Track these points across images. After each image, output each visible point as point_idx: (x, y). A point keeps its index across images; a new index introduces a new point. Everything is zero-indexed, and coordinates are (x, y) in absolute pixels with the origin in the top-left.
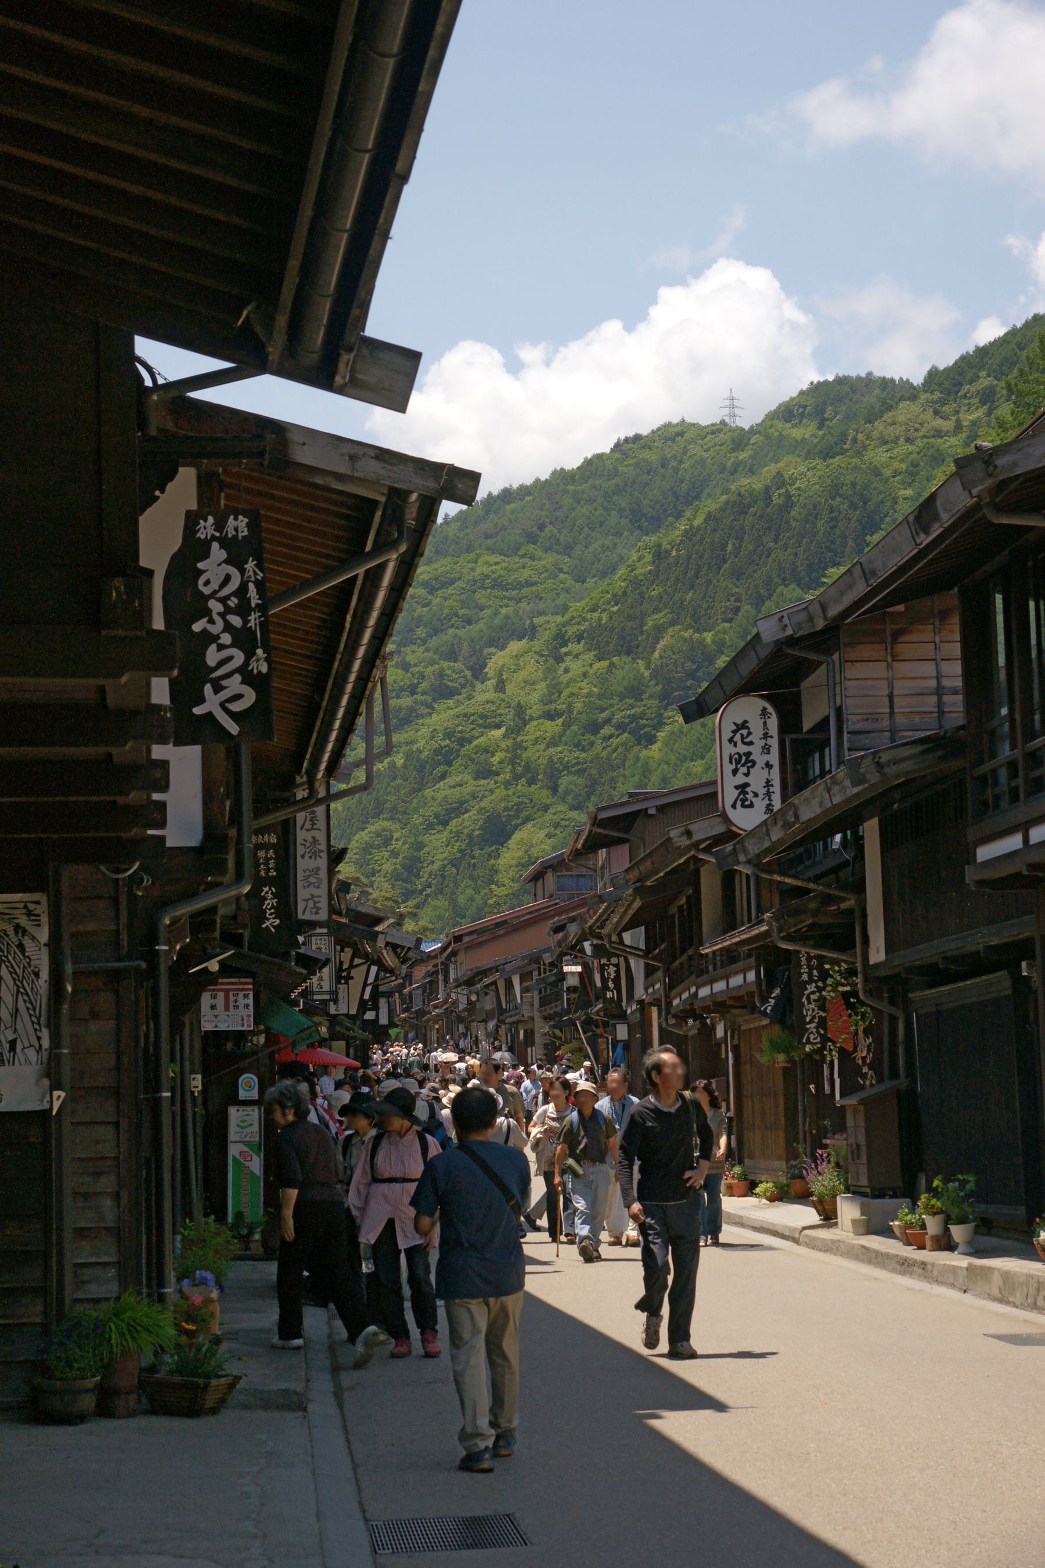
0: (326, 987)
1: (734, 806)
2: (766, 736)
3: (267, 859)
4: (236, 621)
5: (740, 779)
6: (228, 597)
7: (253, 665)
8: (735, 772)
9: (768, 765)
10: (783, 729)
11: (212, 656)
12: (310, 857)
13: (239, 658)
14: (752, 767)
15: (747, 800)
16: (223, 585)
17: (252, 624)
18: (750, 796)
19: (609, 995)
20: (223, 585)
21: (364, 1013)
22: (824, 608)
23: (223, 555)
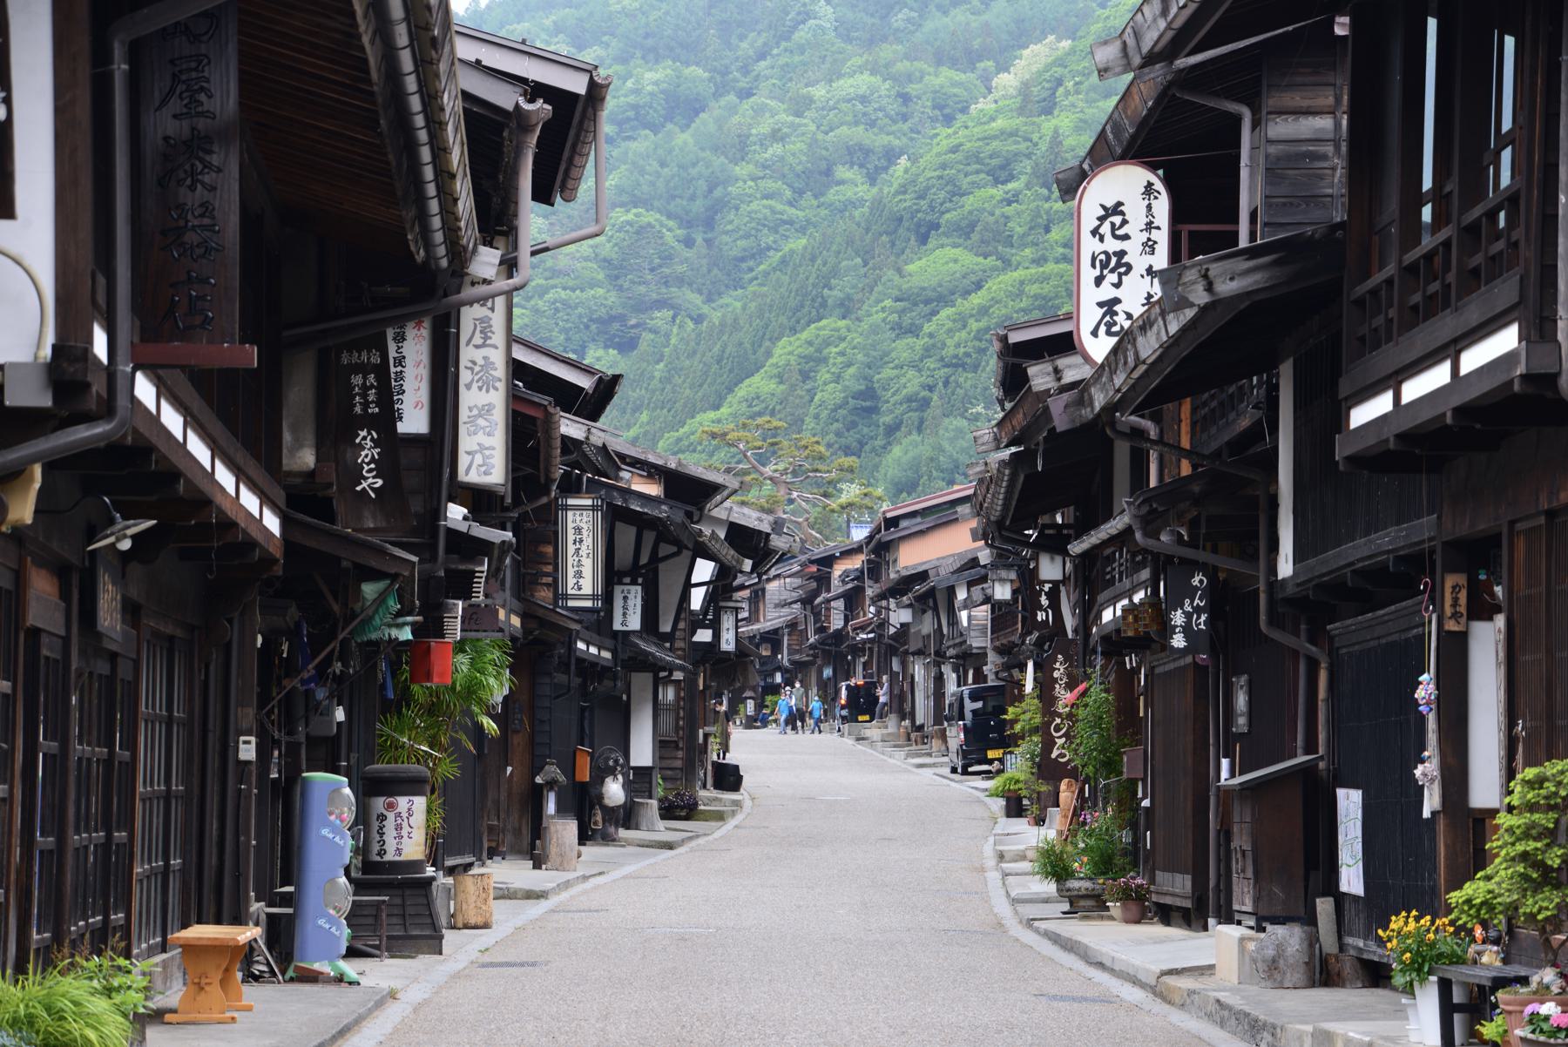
0: (587, 589)
1: (1095, 333)
2: (1150, 226)
3: (365, 388)
5: (1106, 292)
8: (1099, 281)
10: (1176, 216)
12: (480, 389)
14: (1126, 273)
15: (1115, 323)
19: (1041, 616)
21: (694, 633)
22: (1137, 35)
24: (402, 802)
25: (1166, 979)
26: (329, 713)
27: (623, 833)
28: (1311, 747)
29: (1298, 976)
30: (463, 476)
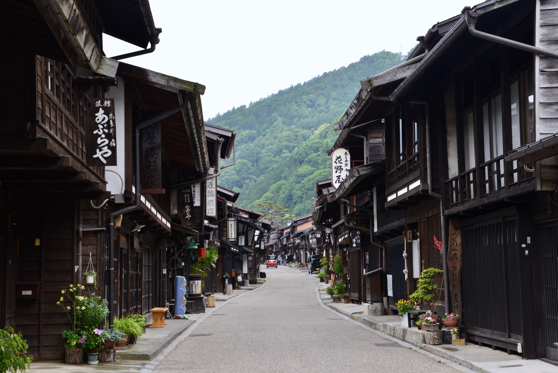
2: (346, 161)
3: (187, 197)
4: (106, 131)
5: (338, 174)
6: (104, 124)
7: (111, 143)
8: (336, 172)
10: (352, 159)
11: (99, 141)
13: (107, 141)
22: (342, 123)
23: (103, 112)
24: (196, 282)
27: (242, 287)
28: (382, 266)
29: (380, 313)
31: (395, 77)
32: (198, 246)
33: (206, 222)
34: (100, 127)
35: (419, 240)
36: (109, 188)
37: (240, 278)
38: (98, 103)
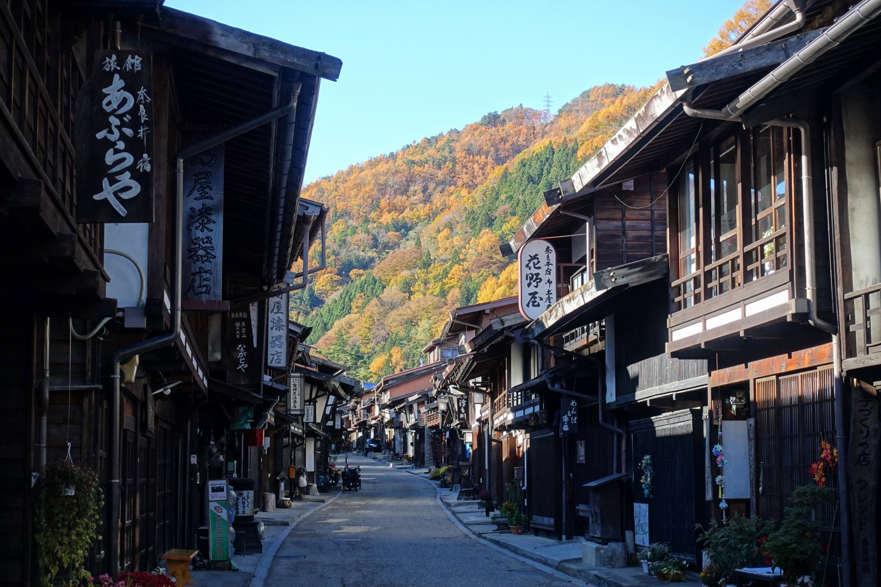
0: (298, 407)
1: (528, 305)
2: (548, 264)
3: (241, 328)
4: (128, 132)
5: (532, 289)
6: (124, 115)
7: (140, 165)
8: (529, 285)
9: (549, 282)
10: (558, 260)
11: (110, 157)
13: (130, 159)
16: (121, 106)
17: (141, 135)
18: (538, 300)
19: (461, 416)
20: (121, 106)
23: (122, 84)
24: (245, 493)
25: (563, 564)
26: (217, 457)
27: (306, 497)
28: (619, 470)
29: (621, 562)
30: (269, 364)
31: (740, 65)
32: (252, 424)
33: (267, 378)
34: (114, 121)
35: (752, 421)
36: (111, 291)
37: (303, 481)
38: (111, 62)
